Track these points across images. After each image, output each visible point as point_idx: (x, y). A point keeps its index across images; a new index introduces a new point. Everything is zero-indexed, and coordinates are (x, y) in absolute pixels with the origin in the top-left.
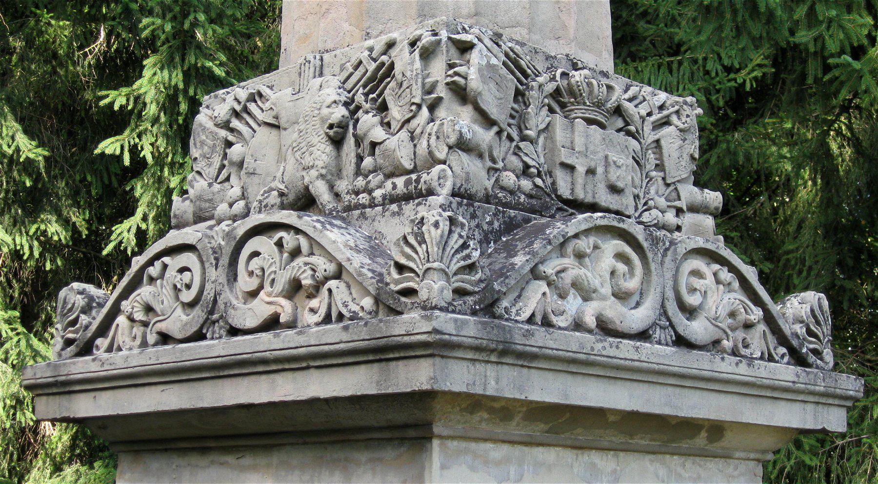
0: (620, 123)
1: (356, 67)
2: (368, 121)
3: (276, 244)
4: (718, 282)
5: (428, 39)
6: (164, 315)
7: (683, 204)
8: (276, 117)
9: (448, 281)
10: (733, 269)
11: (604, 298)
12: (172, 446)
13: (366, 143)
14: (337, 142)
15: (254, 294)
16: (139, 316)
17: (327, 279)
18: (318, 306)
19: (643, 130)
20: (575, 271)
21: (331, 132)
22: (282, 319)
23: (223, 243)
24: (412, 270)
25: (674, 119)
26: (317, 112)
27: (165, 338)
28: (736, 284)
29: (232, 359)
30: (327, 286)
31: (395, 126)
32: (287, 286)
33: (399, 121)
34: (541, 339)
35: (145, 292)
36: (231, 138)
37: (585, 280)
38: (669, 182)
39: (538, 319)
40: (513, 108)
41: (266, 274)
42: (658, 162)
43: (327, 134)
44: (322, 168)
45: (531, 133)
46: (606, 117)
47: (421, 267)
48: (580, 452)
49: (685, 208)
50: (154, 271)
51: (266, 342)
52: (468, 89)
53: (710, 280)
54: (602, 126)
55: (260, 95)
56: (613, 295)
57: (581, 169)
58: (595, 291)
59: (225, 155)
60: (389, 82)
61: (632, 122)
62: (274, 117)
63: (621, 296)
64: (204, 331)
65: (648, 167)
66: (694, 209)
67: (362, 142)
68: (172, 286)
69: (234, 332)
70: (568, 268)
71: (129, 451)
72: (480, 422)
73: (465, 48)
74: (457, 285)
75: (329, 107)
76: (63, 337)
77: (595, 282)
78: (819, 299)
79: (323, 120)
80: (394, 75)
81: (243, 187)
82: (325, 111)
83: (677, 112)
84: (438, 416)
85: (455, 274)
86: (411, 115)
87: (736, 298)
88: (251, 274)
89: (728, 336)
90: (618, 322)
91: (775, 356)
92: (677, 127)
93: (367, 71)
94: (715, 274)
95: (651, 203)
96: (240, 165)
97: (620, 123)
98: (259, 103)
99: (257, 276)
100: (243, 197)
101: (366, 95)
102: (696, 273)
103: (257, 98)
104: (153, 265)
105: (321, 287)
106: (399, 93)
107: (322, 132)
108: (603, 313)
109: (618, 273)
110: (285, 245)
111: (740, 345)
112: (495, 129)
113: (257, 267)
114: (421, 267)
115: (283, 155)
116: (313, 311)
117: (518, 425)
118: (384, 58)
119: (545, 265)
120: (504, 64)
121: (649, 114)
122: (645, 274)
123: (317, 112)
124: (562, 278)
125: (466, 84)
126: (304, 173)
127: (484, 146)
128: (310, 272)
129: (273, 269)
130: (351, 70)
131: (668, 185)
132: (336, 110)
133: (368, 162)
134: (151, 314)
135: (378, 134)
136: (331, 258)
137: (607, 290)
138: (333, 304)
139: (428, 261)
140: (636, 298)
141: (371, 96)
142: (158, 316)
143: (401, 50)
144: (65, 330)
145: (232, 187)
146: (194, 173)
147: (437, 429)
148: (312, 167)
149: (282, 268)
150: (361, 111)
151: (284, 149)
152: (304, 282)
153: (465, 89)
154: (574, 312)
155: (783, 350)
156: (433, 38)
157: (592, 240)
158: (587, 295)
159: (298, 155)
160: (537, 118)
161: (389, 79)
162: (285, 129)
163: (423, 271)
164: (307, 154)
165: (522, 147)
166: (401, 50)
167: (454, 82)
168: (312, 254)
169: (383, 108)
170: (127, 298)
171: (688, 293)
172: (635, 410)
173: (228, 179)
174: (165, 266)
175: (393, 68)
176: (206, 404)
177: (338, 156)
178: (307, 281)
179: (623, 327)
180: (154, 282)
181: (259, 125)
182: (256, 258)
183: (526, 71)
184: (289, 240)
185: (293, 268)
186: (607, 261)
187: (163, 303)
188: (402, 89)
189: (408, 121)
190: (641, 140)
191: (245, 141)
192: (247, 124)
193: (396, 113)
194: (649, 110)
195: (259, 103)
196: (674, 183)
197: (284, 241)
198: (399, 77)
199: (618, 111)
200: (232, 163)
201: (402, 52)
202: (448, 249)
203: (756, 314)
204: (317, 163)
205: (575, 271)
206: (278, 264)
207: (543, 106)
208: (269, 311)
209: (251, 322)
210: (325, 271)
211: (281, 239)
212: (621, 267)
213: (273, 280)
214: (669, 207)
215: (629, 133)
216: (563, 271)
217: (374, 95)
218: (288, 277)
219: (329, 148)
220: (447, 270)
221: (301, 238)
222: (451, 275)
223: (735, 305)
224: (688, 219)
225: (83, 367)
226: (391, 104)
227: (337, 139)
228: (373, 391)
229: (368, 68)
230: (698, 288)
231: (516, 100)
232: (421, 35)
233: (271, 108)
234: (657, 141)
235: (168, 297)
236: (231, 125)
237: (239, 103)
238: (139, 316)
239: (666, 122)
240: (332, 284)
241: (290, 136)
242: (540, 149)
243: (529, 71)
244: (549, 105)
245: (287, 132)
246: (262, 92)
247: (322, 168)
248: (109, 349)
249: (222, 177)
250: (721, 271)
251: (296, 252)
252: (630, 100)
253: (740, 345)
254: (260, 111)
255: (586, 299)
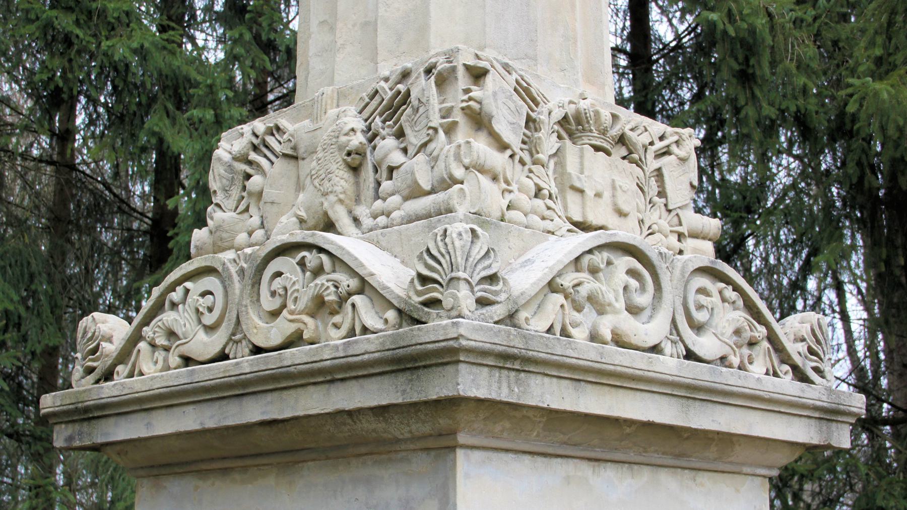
0: (624, 152)
1: (372, 98)
2: (388, 144)
3: (297, 264)
4: (724, 300)
5: (443, 66)
6: (186, 338)
7: (683, 229)
8: (295, 148)
9: (472, 292)
10: (737, 288)
11: (616, 312)
12: (194, 468)
13: (384, 167)
14: (355, 170)
15: (275, 314)
16: (161, 341)
17: (350, 294)
18: (341, 321)
19: (645, 158)
20: (589, 285)
21: (349, 159)
22: (306, 336)
23: (245, 265)
24: (436, 281)
25: (674, 148)
26: (334, 140)
27: (187, 361)
28: (741, 303)
29: (257, 376)
30: (350, 301)
31: (411, 151)
32: (309, 304)
33: (416, 146)
34: (559, 349)
35: (168, 317)
36: (249, 170)
37: (599, 292)
38: (670, 207)
39: (558, 329)
40: (524, 134)
41: (289, 293)
42: (660, 189)
43: (344, 160)
44: (341, 193)
45: (542, 156)
46: (612, 144)
47: (444, 277)
48: (596, 464)
49: (686, 234)
50: (176, 296)
51: (295, 356)
52: (483, 114)
53: (716, 298)
54: (608, 153)
55: (278, 129)
56: (626, 309)
57: (590, 193)
58: (610, 305)
59: (244, 188)
60: (406, 109)
61: (636, 150)
62: (292, 148)
63: (633, 310)
64: (227, 351)
65: (651, 193)
66: (694, 235)
67: (380, 167)
68: (194, 310)
69: (257, 350)
70: (583, 282)
71: (149, 476)
72: (502, 431)
73: (478, 75)
74: (479, 294)
75: (346, 134)
76: (82, 366)
77: (610, 297)
78: (818, 319)
79: (341, 148)
80: (410, 102)
81: (262, 217)
82: (343, 139)
83: (677, 142)
84: (462, 425)
85: (477, 284)
86: (427, 139)
87: (740, 317)
88: (273, 294)
89: (734, 351)
90: (632, 336)
91: (779, 372)
92: (677, 156)
93: (383, 100)
94: (720, 292)
95: (655, 227)
96: (260, 194)
97: (624, 152)
98: (277, 136)
99: (280, 295)
100: (262, 226)
101: (384, 122)
102: (702, 291)
103: (275, 132)
104: (174, 291)
105: (344, 303)
106: (415, 119)
107: (340, 159)
108: (618, 326)
109: (630, 288)
110: (308, 264)
111: (746, 361)
112: (509, 152)
113: (279, 286)
114: (444, 277)
115: (301, 184)
116: (336, 326)
117: (538, 435)
118: (401, 87)
119: (562, 277)
120: (515, 90)
121: (652, 144)
122: (655, 290)
123: (334, 140)
124: (578, 292)
125: (481, 109)
126: (323, 199)
127: (499, 169)
128: (333, 289)
129: (296, 287)
130: (367, 100)
131: (670, 211)
132: (354, 137)
133: (386, 185)
134: (172, 339)
135: (397, 158)
136: (353, 273)
137: (621, 305)
138: (357, 319)
139: (452, 271)
140: (647, 313)
141: (388, 123)
142: (179, 339)
143: (417, 78)
144: (84, 359)
145: (251, 216)
146: (213, 205)
147: (462, 438)
148: (331, 192)
149: (305, 286)
150: (378, 138)
151: (302, 178)
152: (326, 299)
153: (480, 114)
154: (590, 325)
155: (786, 368)
156: (448, 65)
157: (605, 255)
158: (601, 308)
159: (316, 182)
160: (549, 143)
161: (405, 107)
162: (303, 159)
163: (446, 281)
164: (326, 181)
165: (534, 170)
166: (417, 78)
167: (469, 107)
168: (334, 271)
169: (400, 134)
170: (147, 324)
171: (697, 310)
172: (651, 420)
173: (247, 210)
174: (187, 291)
175: (409, 95)
176: (230, 422)
177: (357, 184)
178: (331, 297)
179: (634, 341)
180: (175, 308)
181: (277, 157)
182: (279, 278)
183: (536, 99)
184: (311, 258)
185: (316, 285)
186: (621, 277)
187: (185, 326)
188: (418, 115)
189: (425, 145)
190: (644, 167)
191: (263, 173)
192: (265, 156)
193: (414, 139)
194: (650, 140)
195: (277, 136)
196: (675, 209)
197: (306, 259)
198: (415, 103)
199: (622, 140)
200: (250, 194)
201: (418, 80)
202: (471, 259)
203: (760, 332)
204: (336, 188)
205: (589, 285)
206: (301, 283)
207: (553, 132)
208: (291, 328)
209: (276, 341)
210: (348, 286)
211: (304, 257)
212: (634, 283)
213: (296, 298)
214: (671, 231)
215: (632, 161)
216: (578, 285)
217: (391, 123)
218: (311, 294)
219: (347, 175)
220: (470, 279)
221: (324, 257)
222: (474, 284)
223: (740, 323)
224: (690, 243)
225: (109, 391)
226: (408, 131)
227: (354, 166)
228: (400, 401)
229: (384, 97)
230: (705, 304)
231: (527, 126)
232: (436, 63)
233: (289, 140)
234: (659, 170)
235: (190, 320)
236: (250, 158)
237: (257, 136)
238: (161, 341)
239: (666, 152)
240: (356, 299)
241: (308, 166)
242: (550, 173)
243: (539, 99)
244: (558, 132)
245: (305, 161)
246: (280, 125)
247: (341, 193)
248: (131, 375)
249: (242, 207)
250: (725, 290)
251: (318, 271)
252: (632, 130)
253: (746, 361)
254: (277, 143)
255: (601, 312)
